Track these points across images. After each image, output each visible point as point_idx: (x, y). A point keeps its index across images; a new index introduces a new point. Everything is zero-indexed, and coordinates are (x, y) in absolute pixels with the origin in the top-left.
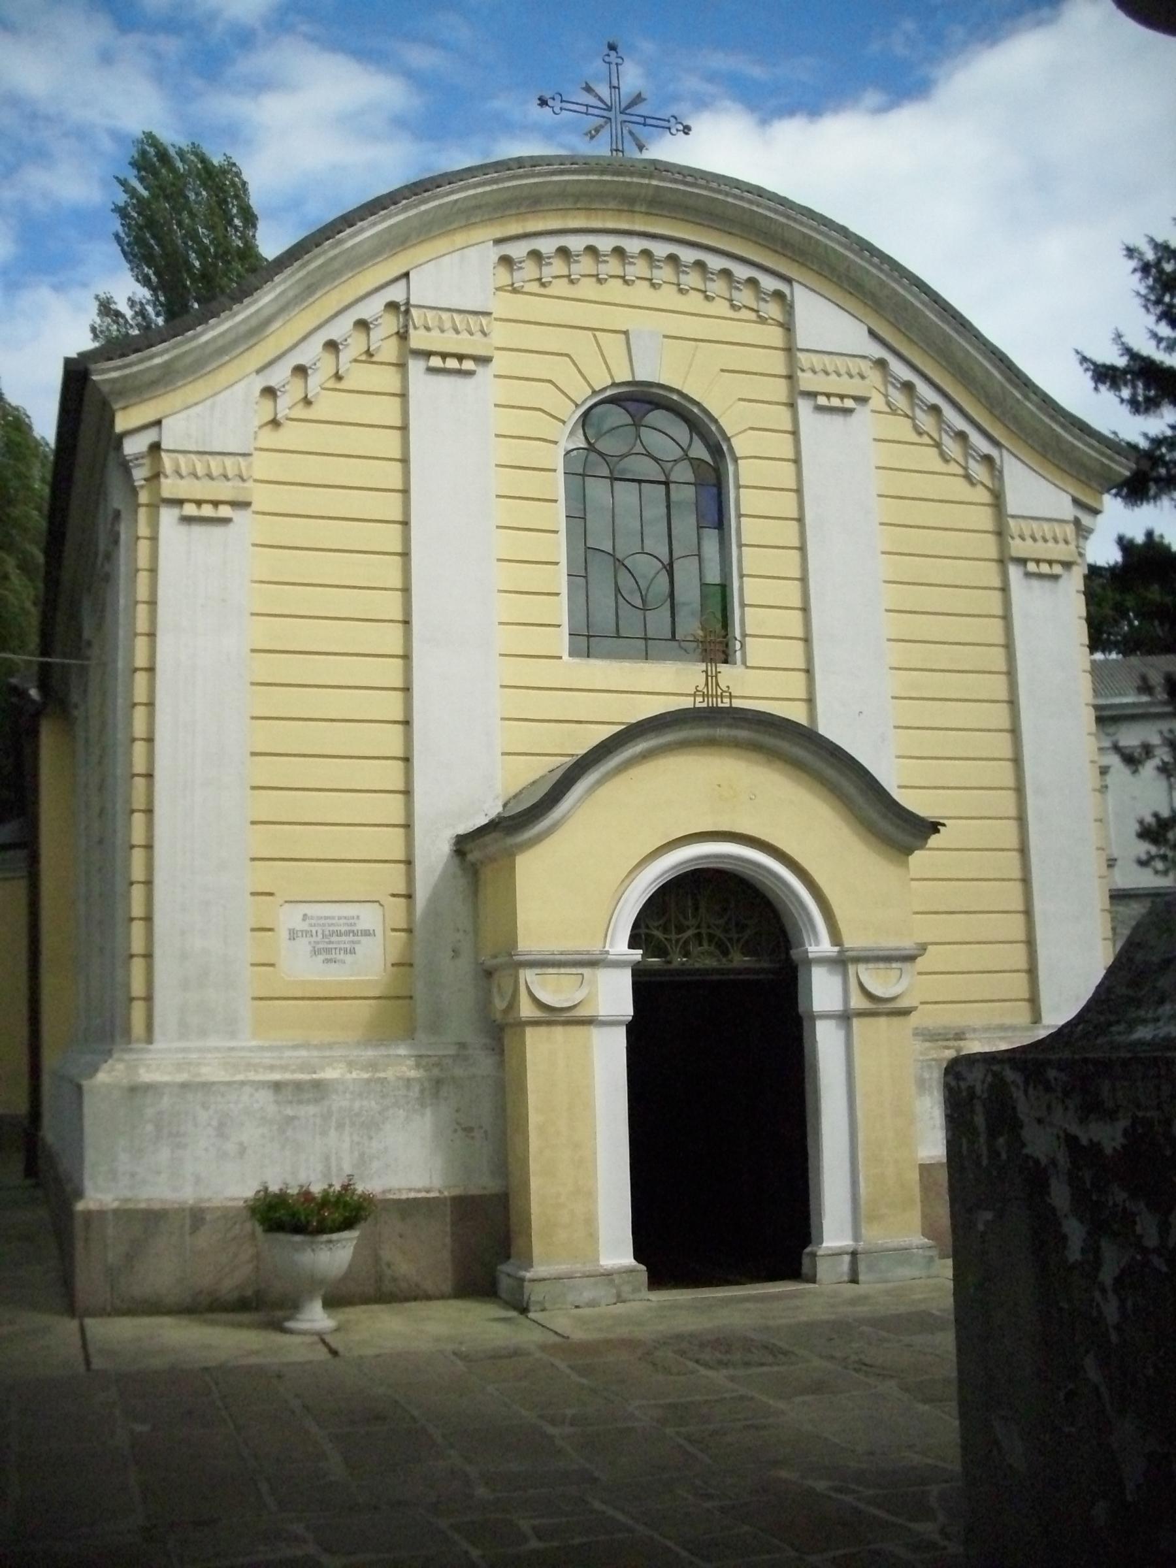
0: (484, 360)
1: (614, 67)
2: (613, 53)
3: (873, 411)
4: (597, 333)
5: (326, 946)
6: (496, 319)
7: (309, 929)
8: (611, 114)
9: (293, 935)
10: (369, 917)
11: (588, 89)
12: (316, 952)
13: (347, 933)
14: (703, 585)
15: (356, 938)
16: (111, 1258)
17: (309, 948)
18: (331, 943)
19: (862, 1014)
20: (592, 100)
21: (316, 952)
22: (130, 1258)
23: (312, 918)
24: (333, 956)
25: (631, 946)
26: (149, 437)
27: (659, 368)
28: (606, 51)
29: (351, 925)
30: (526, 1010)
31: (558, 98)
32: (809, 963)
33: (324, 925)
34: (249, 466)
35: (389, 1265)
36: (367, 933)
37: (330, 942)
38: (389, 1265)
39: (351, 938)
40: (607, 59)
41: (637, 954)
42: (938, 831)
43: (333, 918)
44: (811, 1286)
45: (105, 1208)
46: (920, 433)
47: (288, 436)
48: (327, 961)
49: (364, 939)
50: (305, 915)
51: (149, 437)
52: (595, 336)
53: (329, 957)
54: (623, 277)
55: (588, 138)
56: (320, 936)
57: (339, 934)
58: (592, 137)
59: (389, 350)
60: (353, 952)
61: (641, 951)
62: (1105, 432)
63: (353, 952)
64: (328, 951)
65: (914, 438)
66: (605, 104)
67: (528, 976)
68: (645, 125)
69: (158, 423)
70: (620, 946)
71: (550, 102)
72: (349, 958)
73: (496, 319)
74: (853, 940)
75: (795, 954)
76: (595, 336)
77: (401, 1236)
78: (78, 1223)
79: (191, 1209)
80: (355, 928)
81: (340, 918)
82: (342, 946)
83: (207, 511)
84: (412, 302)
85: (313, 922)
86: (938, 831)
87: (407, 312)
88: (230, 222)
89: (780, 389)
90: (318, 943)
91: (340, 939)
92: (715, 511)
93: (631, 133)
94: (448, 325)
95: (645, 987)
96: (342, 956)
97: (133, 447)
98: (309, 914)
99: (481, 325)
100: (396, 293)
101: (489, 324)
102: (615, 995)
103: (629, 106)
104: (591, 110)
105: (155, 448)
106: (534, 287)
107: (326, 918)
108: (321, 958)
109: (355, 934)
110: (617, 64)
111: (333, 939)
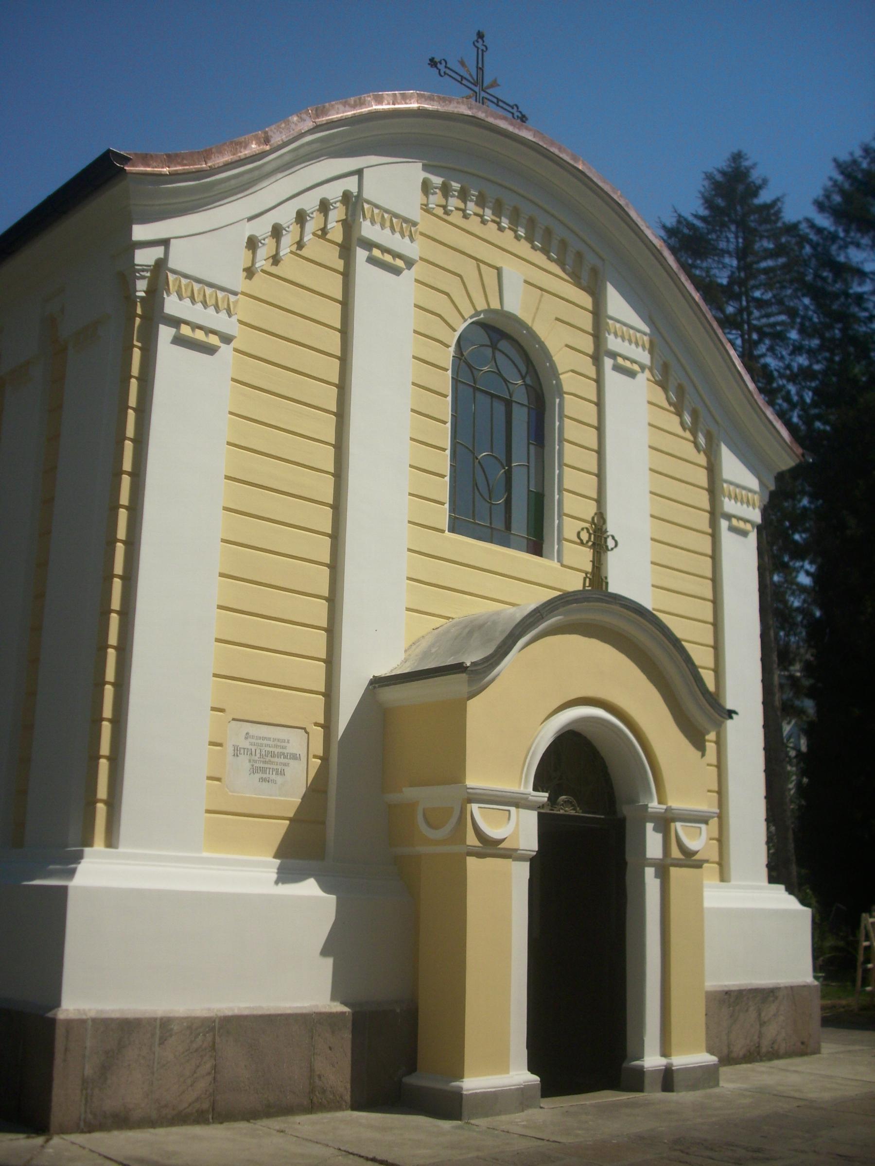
0: (410, 263)
2: (480, 40)
3: (236, 350)
5: (262, 765)
6: (422, 234)
7: (250, 747)
8: (477, 89)
9: (237, 751)
10: (295, 742)
11: (462, 63)
12: (254, 770)
13: (280, 755)
14: (529, 491)
15: (286, 761)
16: (88, 1071)
17: (248, 765)
18: (266, 764)
19: (679, 864)
20: (463, 72)
21: (254, 770)
22: (105, 1069)
23: (253, 737)
24: (267, 776)
25: (535, 789)
26: (158, 252)
27: (516, 302)
29: (283, 748)
30: (472, 839)
32: (644, 815)
33: (262, 745)
34: (236, 302)
35: (320, 1077)
36: (295, 757)
37: (265, 762)
38: (320, 1077)
39: (282, 760)
41: (543, 797)
42: (731, 718)
43: (269, 739)
44: (641, 1094)
45: (84, 1017)
46: (670, 404)
47: (260, 285)
48: (262, 780)
49: (292, 762)
50: (247, 734)
51: (158, 252)
53: (264, 776)
56: (258, 755)
57: (273, 755)
59: (336, 233)
60: (282, 773)
61: (547, 795)
63: (282, 773)
64: (263, 770)
65: (665, 404)
67: (475, 807)
68: (498, 105)
69: (165, 243)
70: (525, 787)
71: (439, 65)
72: (279, 779)
73: (422, 234)
74: (676, 803)
75: (626, 810)
77: (330, 1048)
78: (60, 1032)
79: (161, 1019)
80: (285, 751)
81: (274, 740)
82: (275, 767)
83: (199, 335)
84: (366, 195)
85: (253, 741)
86: (731, 718)
87: (355, 204)
89: (587, 344)
90: (255, 761)
91: (272, 759)
92: (540, 432)
94: (397, 229)
95: (549, 827)
96: (273, 777)
97: (144, 258)
98: (251, 734)
99: (411, 231)
100: (351, 183)
102: (522, 830)
103: (488, 87)
104: (464, 82)
105: (160, 265)
106: (440, 211)
107: (264, 738)
108: (258, 776)
109: (285, 757)
111: (269, 758)
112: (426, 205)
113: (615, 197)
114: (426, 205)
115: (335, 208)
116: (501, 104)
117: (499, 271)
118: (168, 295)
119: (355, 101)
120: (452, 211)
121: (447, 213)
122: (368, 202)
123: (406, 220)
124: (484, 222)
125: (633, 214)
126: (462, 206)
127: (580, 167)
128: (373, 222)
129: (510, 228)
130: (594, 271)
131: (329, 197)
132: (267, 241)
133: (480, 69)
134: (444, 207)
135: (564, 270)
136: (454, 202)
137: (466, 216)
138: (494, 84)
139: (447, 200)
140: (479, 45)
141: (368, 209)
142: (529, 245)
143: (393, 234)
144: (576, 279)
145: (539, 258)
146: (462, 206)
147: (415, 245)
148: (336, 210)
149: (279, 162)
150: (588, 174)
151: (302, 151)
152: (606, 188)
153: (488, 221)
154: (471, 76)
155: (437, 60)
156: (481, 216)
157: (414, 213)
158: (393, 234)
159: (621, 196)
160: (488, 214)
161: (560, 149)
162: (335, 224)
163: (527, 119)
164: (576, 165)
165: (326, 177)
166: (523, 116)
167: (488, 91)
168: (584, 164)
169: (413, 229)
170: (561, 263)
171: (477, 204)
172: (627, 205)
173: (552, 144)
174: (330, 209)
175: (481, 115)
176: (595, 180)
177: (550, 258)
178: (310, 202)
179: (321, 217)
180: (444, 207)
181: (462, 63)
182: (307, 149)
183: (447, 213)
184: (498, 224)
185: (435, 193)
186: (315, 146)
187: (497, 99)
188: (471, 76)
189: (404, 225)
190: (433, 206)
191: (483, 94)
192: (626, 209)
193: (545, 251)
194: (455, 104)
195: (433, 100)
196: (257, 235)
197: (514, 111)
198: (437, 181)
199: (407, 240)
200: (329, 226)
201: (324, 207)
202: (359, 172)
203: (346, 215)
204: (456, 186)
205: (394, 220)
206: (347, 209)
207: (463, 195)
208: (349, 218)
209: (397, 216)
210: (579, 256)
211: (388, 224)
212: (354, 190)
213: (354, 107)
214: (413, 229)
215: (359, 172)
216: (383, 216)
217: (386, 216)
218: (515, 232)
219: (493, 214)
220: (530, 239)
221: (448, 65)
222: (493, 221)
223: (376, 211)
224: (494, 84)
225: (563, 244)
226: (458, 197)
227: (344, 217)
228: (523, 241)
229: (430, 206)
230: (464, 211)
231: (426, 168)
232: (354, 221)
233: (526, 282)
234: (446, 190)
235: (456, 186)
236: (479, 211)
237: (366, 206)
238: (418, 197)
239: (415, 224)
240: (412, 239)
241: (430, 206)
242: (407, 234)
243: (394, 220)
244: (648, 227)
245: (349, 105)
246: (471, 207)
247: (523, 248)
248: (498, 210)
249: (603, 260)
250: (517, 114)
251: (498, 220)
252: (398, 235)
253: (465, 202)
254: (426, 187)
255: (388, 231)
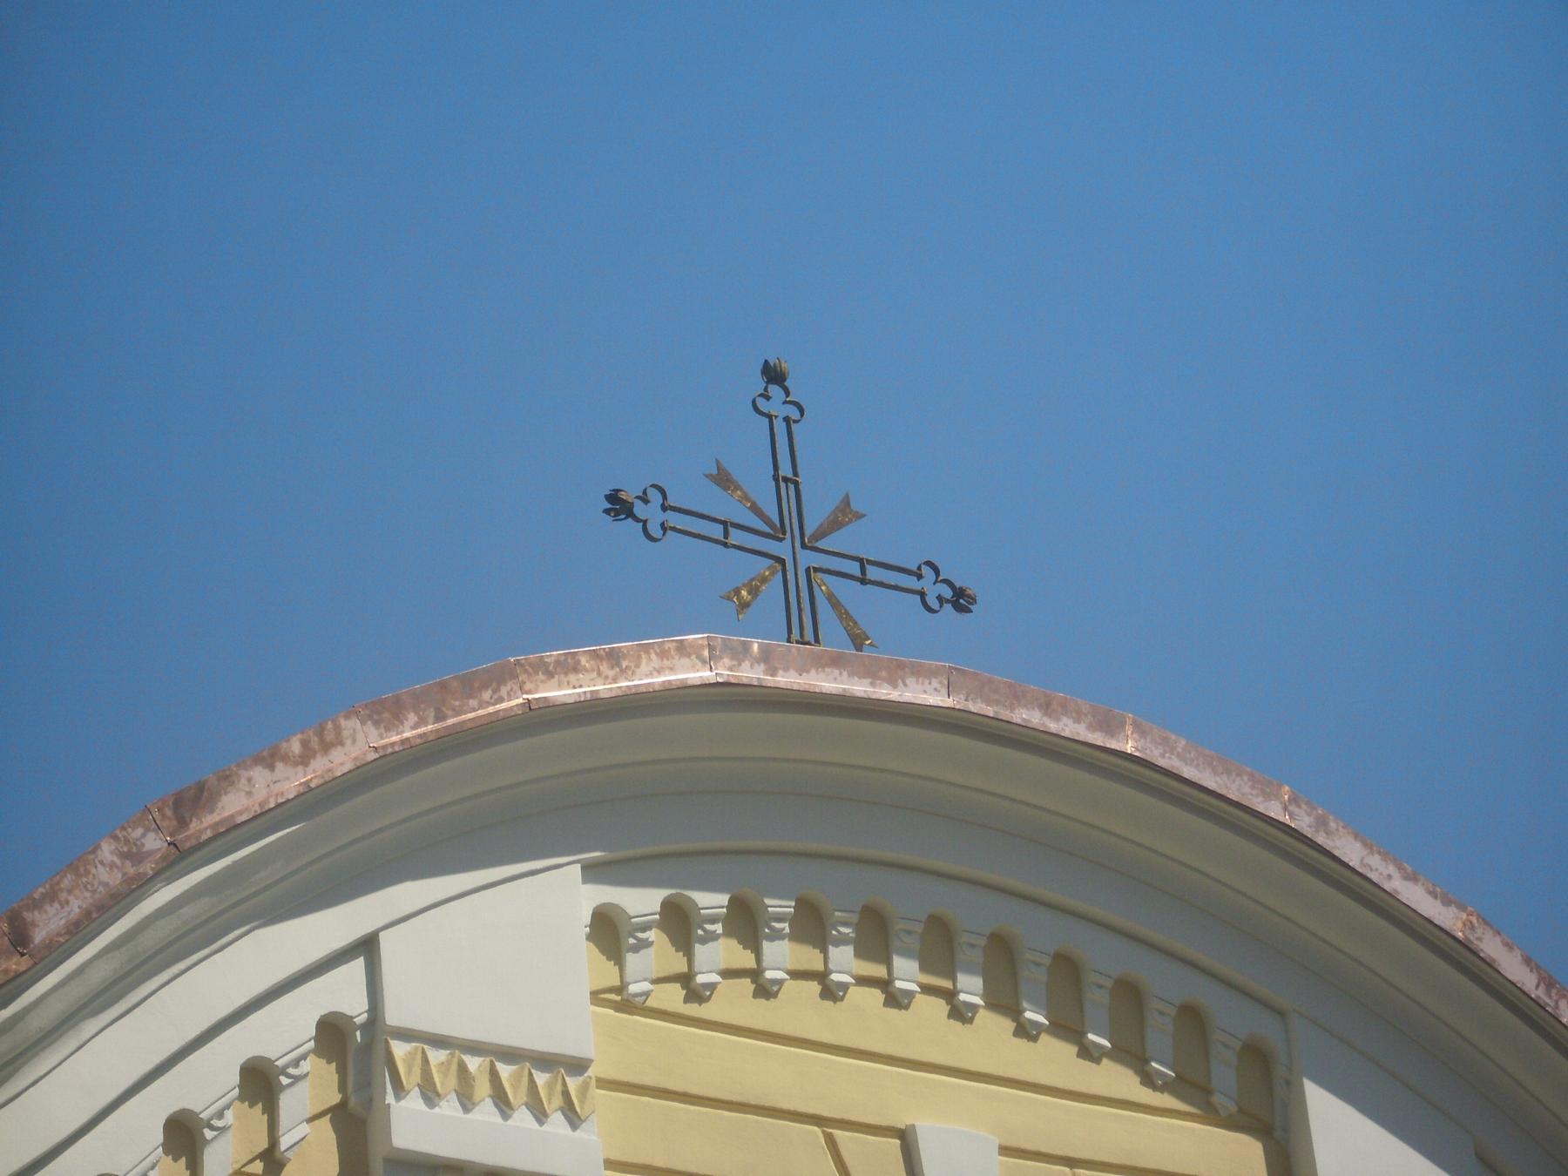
1: (780, 427)
2: (774, 390)
4: (837, 1133)
6: (605, 1084)
8: (782, 549)
11: (723, 479)
28: (759, 383)
31: (655, 496)
40: (761, 402)
52: (831, 1142)
54: (821, 977)
55: (731, 607)
58: (744, 606)
62: (265, 1117)
66: (768, 521)
68: (863, 581)
71: (640, 509)
73: (605, 1084)
76: (831, 1142)
84: (394, 1015)
87: (367, 1049)
88: (1479, 916)
93: (835, 603)
94: (517, 1096)
99: (566, 1094)
100: (343, 992)
101: (584, 1090)
103: (821, 533)
104: (736, 537)
106: (672, 997)
110: (787, 420)
112: (620, 990)
113: (1274, 810)
114: (620, 990)
115: (297, 1079)
116: (873, 573)
117: (906, 1139)
118: (398, 1097)
119: (305, 744)
120: (712, 987)
121: (696, 994)
122: (406, 1035)
123: (546, 1061)
124: (831, 993)
125: (1350, 850)
126: (746, 959)
127: (1129, 748)
128: (430, 1095)
129: (927, 989)
130: (1256, 1057)
131: (271, 1052)
132: (305, 1066)
133: (787, 483)
134: (686, 979)
135: (1148, 1080)
136: (717, 954)
137: (765, 991)
138: (844, 514)
139: (689, 955)
140: (776, 406)
141: (410, 1057)
142: (1008, 1025)
143: (506, 1117)
144: (1195, 1092)
145: (1053, 1059)
146: (746, 959)
147: (589, 1134)
148: (303, 1086)
149: (77, 992)
150: (1162, 762)
151: (150, 939)
152: (1236, 788)
153: (845, 987)
154: (755, 509)
155: (629, 495)
156: (821, 977)
157: (577, 1027)
158: (506, 1117)
159: (1294, 800)
160: (844, 962)
161: (1047, 707)
162: (305, 1128)
163: (973, 600)
164: (1113, 744)
165: (260, 985)
166: (959, 593)
167: (819, 545)
168: (1141, 731)
169: (573, 1084)
170: (1132, 1055)
171: (797, 936)
172: (1321, 823)
173: (1017, 697)
174: (207, 1142)
175: (750, 673)
176: (1188, 772)
177: (1088, 1053)
178: (208, 1083)
179: (258, 1116)
180: (686, 979)
181: (723, 479)
182: (165, 928)
183: (696, 994)
184: (885, 985)
185: (645, 944)
186: (188, 911)
187: (861, 561)
188: (755, 509)
189: (541, 1078)
190: (645, 986)
191: (807, 559)
192: (1320, 839)
193: (1068, 1028)
194: (656, 661)
195: (576, 669)
196: (272, 1055)
197: (928, 583)
198: (642, 902)
199: (557, 1121)
200: (285, 1142)
201: (260, 1083)
202: (367, 947)
203: (342, 1087)
204: (711, 901)
205: (505, 1071)
206: (342, 1071)
207: (746, 923)
208: (352, 1102)
209: (510, 1055)
210: (1192, 1018)
211: (483, 1088)
212: (355, 1006)
213: (304, 760)
214: (573, 1084)
215: (367, 947)
216: (462, 1068)
217: (473, 1063)
218: (950, 996)
219: (860, 954)
220: (1004, 1001)
221: (671, 502)
222: (863, 981)
223: (437, 1056)
224: (844, 514)
225: (1130, 995)
226: (728, 933)
227: (336, 1098)
228: (985, 1018)
229: (633, 988)
230: (755, 974)
231: (593, 873)
232: (369, 1103)
233: (1005, 1150)
234: (679, 923)
235: (711, 901)
236: (810, 958)
237: (400, 1049)
238: (587, 967)
239: (578, 1066)
240: (573, 1117)
241: (633, 988)
242: (553, 1104)
243: (505, 1071)
244: (1412, 878)
245: (285, 759)
246: (780, 955)
247: (990, 1039)
248: (876, 938)
249: (1281, 1013)
250: (933, 591)
251: (879, 971)
252: (523, 1118)
253: (752, 941)
254: (608, 931)
255: (486, 1111)
